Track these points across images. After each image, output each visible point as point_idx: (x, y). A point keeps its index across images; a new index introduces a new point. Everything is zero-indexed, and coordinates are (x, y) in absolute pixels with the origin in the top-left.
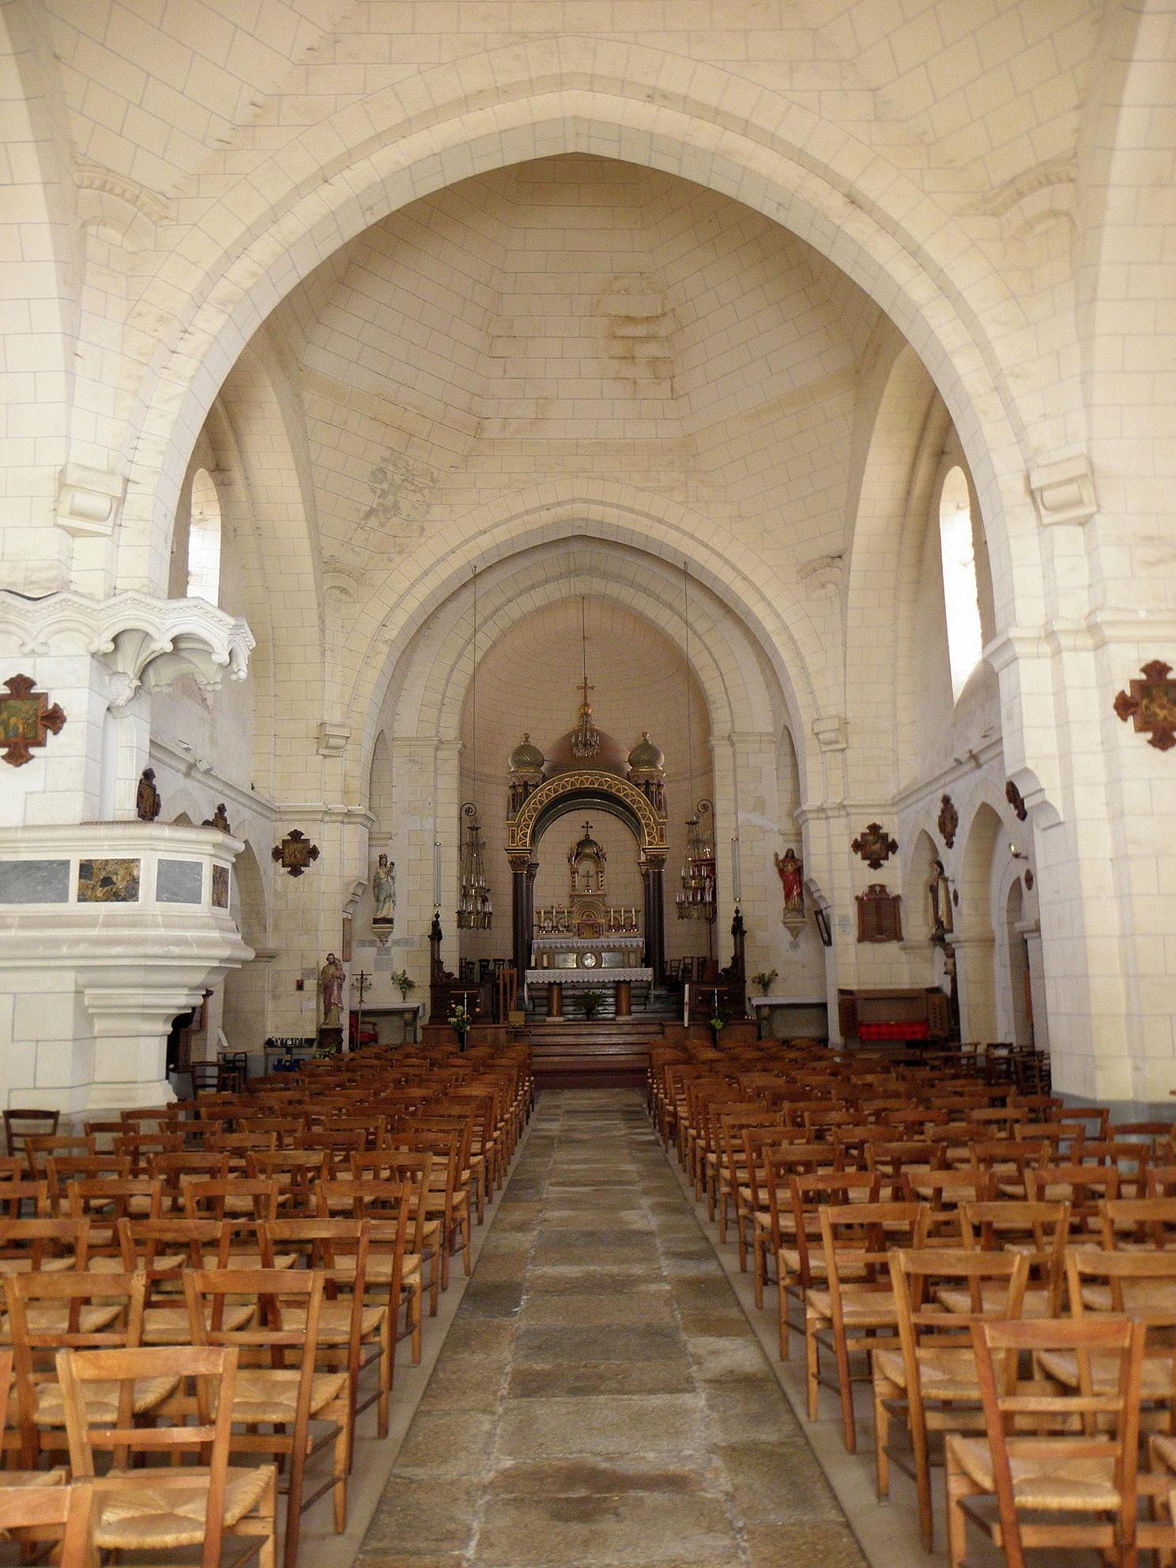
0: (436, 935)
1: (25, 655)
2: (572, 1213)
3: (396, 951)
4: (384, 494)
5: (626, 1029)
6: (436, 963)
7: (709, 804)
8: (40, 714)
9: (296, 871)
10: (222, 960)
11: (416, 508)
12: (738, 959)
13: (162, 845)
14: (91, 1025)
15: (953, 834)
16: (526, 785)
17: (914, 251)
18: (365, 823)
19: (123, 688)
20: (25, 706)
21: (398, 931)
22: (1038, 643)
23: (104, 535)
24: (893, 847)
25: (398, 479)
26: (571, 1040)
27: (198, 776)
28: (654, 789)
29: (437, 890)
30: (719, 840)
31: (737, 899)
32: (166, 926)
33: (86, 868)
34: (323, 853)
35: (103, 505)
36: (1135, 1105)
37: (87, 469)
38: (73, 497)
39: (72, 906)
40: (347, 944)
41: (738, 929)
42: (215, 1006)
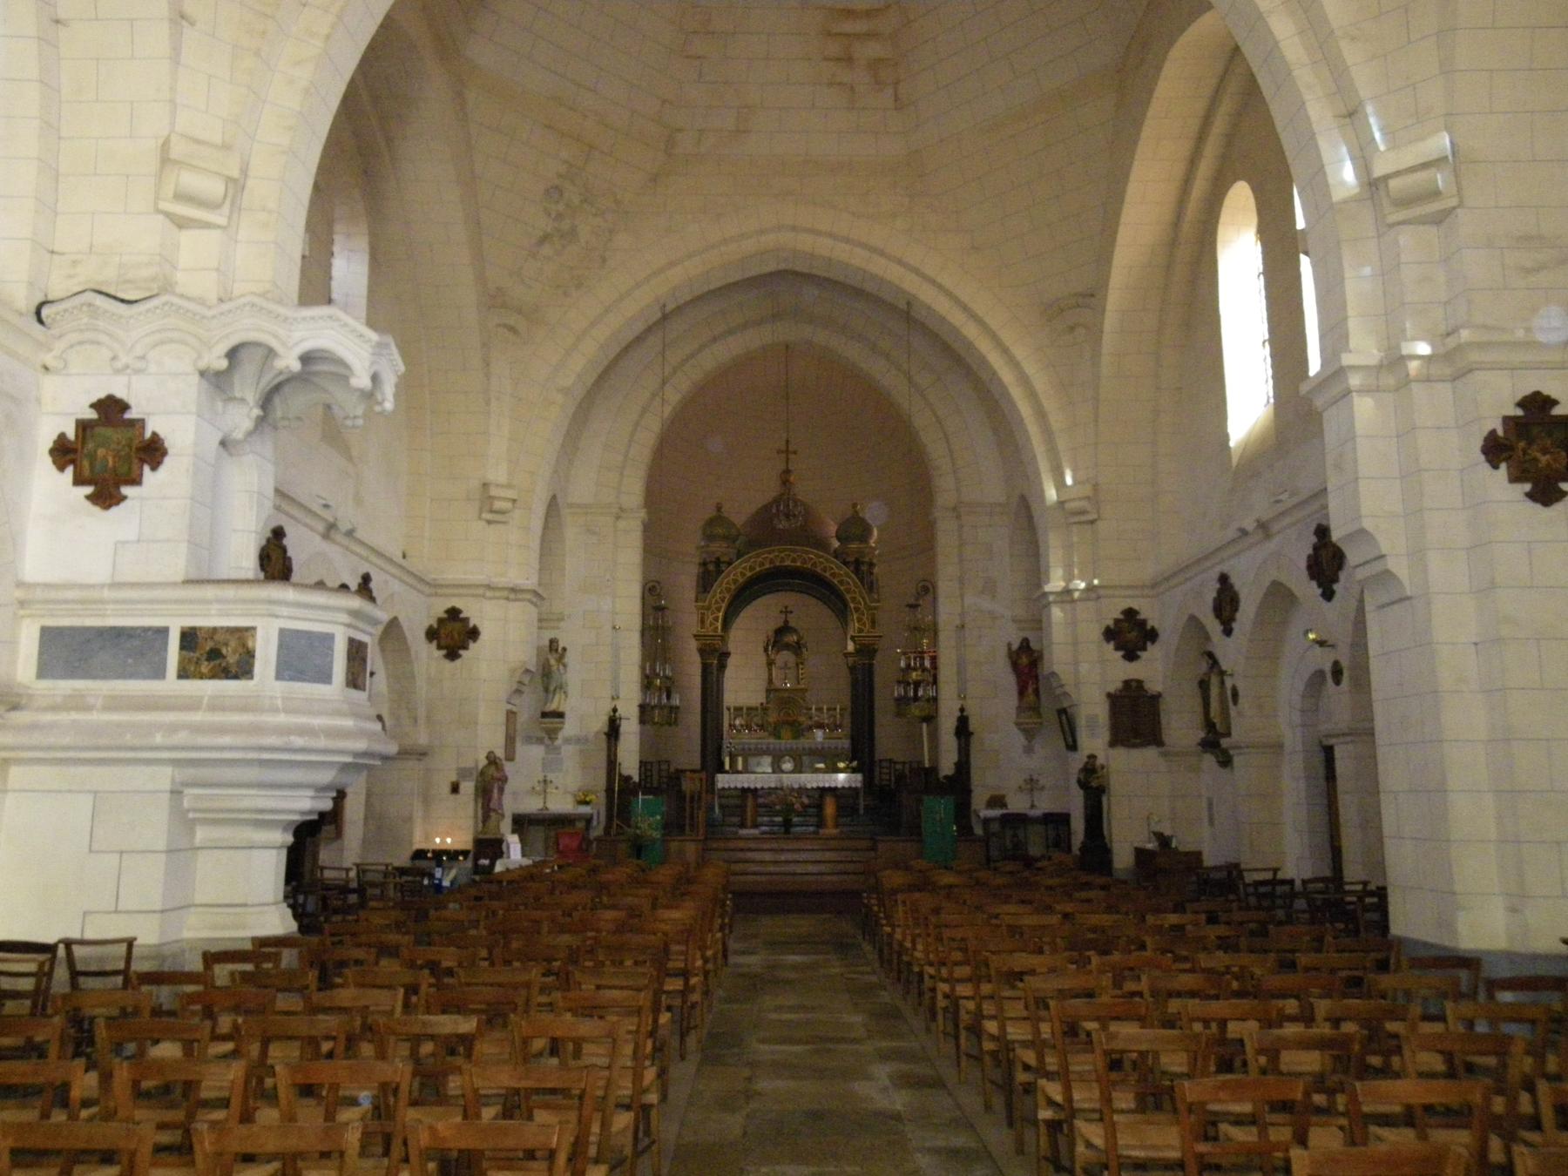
0: (613, 730)
1: (118, 372)
2: (792, 1084)
3: (569, 752)
4: (559, 216)
5: (833, 844)
6: (612, 763)
7: (930, 587)
8: (136, 443)
9: (452, 655)
10: (356, 755)
13: (285, 611)
14: (192, 833)
15: (1232, 619)
16: (718, 562)
18: (534, 600)
19: (241, 418)
21: (569, 728)
22: (1378, 372)
23: (219, 227)
24: (1152, 635)
25: (576, 201)
26: (768, 857)
27: (339, 538)
28: (864, 568)
29: (615, 680)
30: (941, 625)
31: (962, 696)
32: (287, 711)
33: (189, 638)
34: (485, 636)
35: (215, 188)
36: (1510, 956)
37: (198, 141)
38: (178, 175)
39: (171, 685)
40: (510, 740)
41: (963, 729)
42: (354, 811)
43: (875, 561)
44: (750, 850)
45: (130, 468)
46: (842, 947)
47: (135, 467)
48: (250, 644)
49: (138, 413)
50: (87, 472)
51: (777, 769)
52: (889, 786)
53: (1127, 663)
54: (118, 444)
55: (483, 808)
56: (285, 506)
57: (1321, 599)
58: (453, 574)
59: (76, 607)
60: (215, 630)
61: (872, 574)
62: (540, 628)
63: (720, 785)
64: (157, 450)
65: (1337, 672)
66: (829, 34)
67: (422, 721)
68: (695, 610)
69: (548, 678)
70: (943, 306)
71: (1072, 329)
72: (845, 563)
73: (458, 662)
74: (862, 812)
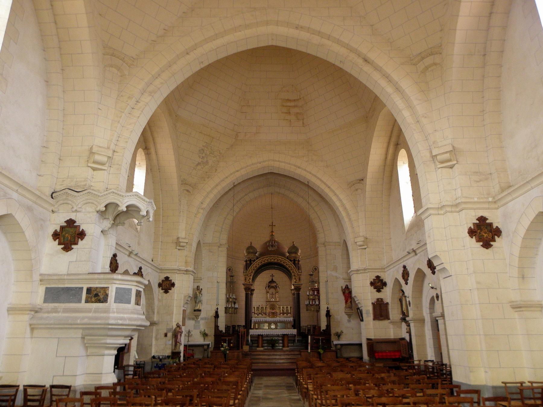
0: (217, 316)
1: (73, 212)
3: (202, 322)
5: (287, 353)
6: (217, 327)
7: (317, 268)
8: (77, 232)
9: (166, 292)
11: (214, 163)
12: (328, 326)
13: (118, 282)
15: (407, 280)
16: (250, 261)
17: (387, 77)
19: (107, 224)
20: (72, 230)
21: (203, 315)
25: (208, 153)
28: (297, 262)
29: (218, 299)
31: (328, 303)
32: (118, 313)
33: (89, 290)
35: (105, 159)
39: (83, 305)
41: (328, 314)
43: (300, 260)
44: (260, 355)
45: (75, 240)
46: (289, 388)
47: (76, 239)
48: (107, 292)
49: (78, 224)
50: (62, 241)
51: (269, 328)
52: (305, 332)
53: (378, 293)
54: (72, 232)
55: (175, 342)
56: (119, 248)
57: (431, 274)
58: (168, 266)
59: (56, 281)
60: (97, 288)
61: (299, 264)
62: (194, 282)
63: (251, 334)
64: (83, 234)
65: (437, 297)
66: (283, 106)
67: (156, 313)
68: (243, 275)
69: (196, 299)
70: (318, 183)
71: (357, 190)
72: (291, 261)
73: (168, 294)
74: (296, 342)
